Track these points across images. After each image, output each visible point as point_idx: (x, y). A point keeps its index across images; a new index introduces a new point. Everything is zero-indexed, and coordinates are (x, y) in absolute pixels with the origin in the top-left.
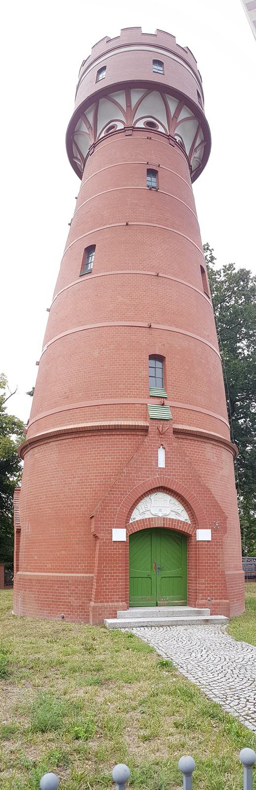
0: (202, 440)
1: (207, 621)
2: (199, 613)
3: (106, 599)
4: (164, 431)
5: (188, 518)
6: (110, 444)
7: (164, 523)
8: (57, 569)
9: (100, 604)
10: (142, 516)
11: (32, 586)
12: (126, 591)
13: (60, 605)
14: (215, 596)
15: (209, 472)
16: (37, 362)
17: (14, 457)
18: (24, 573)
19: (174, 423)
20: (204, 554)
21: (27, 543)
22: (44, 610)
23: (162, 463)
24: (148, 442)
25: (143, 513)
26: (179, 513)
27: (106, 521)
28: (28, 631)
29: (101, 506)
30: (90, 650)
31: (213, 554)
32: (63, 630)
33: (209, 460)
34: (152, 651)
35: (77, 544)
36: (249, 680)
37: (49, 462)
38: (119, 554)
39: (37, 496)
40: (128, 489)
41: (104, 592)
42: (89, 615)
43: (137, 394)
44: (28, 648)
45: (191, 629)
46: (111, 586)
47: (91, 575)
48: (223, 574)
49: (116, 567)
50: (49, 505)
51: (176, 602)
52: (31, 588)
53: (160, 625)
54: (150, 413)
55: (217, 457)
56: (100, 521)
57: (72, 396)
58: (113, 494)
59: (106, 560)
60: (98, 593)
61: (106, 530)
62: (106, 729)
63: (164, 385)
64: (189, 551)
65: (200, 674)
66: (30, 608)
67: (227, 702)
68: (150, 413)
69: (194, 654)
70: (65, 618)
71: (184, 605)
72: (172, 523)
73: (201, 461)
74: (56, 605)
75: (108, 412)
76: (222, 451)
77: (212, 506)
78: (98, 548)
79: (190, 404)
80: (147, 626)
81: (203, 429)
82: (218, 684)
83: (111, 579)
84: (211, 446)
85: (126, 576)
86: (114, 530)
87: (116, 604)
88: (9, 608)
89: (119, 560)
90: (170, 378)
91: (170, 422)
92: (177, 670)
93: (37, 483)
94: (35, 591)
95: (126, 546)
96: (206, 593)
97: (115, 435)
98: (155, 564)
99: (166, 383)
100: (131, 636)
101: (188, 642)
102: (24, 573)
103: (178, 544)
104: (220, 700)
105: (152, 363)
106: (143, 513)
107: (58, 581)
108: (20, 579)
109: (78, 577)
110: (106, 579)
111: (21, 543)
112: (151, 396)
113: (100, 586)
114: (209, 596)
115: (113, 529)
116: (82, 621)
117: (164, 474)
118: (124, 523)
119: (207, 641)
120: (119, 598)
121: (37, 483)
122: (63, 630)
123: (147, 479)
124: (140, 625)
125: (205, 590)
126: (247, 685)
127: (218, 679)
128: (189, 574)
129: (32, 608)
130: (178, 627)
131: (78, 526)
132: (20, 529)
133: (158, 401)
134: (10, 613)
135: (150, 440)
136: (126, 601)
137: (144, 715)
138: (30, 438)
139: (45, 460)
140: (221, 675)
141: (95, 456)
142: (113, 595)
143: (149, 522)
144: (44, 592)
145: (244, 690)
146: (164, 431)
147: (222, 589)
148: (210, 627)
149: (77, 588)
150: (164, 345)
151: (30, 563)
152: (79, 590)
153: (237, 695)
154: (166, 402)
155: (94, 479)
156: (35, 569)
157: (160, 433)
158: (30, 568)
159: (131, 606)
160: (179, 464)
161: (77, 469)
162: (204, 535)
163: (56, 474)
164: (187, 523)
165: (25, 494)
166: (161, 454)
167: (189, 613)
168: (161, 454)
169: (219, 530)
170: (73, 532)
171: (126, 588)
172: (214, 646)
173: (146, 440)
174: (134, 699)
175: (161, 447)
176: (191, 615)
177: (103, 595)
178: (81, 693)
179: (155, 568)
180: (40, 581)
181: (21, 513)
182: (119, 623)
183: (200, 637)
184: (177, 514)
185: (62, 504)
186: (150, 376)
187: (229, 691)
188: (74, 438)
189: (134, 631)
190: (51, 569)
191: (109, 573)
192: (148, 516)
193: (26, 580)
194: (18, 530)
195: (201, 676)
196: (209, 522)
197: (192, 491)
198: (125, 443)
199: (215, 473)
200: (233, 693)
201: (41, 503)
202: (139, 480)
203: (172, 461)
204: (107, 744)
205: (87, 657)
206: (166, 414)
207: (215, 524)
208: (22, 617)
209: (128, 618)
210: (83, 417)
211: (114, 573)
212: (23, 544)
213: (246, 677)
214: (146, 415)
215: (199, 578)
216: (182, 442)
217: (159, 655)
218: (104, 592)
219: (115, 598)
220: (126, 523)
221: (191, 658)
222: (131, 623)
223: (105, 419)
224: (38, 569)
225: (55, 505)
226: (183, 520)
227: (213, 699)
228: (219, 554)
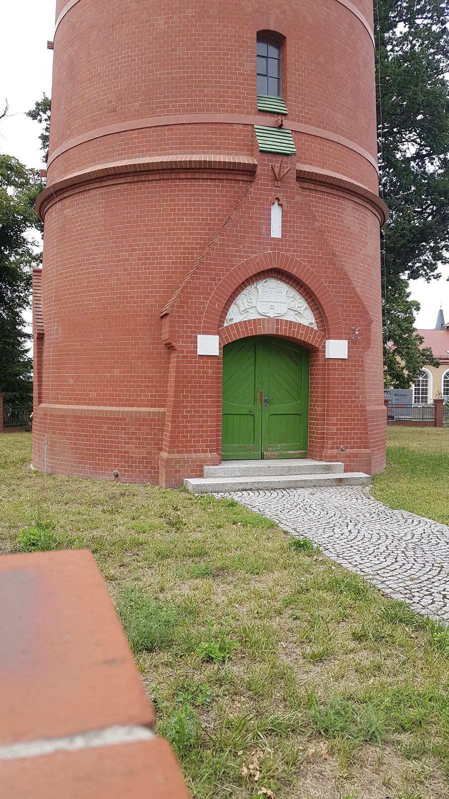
0: (340, 193)
1: (340, 481)
2: (328, 469)
4: (282, 174)
5: (313, 321)
6: (191, 195)
7: (277, 329)
8: (107, 400)
9: (177, 456)
10: (244, 316)
11: (66, 425)
12: (218, 436)
13: (111, 456)
14: (350, 443)
15: (346, 249)
16: (49, 43)
17: (15, 220)
18: (52, 406)
19: (298, 161)
20: (337, 379)
21: (56, 355)
22: (86, 463)
23: (276, 231)
24: (255, 194)
25: (246, 311)
26: (301, 312)
27: (187, 322)
28: (68, 495)
29: (179, 297)
30: (176, 525)
31: (349, 379)
32: (123, 495)
33: (348, 228)
34: (273, 526)
35: (139, 358)
36: (433, 565)
37: (89, 223)
38: (208, 377)
39: (73, 280)
40: (222, 270)
41: (183, 437)
42: (157, 473)
43: (236, 107)
44: (78, 522)
45: (320, 494)
47: (162, 410)
48: (363, 410)
49: (202, 397)
50: (92, 296)
51: (292, 452)
52: (64, 430)
53: (271, 488)
54: (259, 141)
55: (359, 224)
56: (178, 322)
57: (122, 108)
58: (198, 279)
59: (187, 387)
60: (173, 439)
62: (249, 646)
63: (282, 91)
64: (312, 374)
65: (357, 558)
66: (62, 460)
67: (416, 599)
68: (259, 141)
69: (337, 530)
71: (304, 457)
72: (290, 329)
73: (337, 229)
74: (105, 456)
75: (188, 138)
76: (367, 215)
77: (350, 302)
78: (173, 364)
79: (325, 128)
80: (251, 490)
81: (342, 174)
82: (391, 573)
83: (194, 416)
84: (352, 205)
85: (218, 411)
86: (200, 337)
87: (202, 455)
88: (23, 461)
89: (208, 387)
90: (293, 78)
91: (292, 158)
92: (319, 552)
93: (71, 258)
94: (70, 435)
95: (218, 363)
96: (338, 439)
97: (199, 179)
98: (261, 393)
99: (286, 87)
100: (233, 504)
101: (322, 512)
102: (52, 406)
103: (295, 362)
104: (403, 596)
105: (262, 48)
106: (246, 311)
107: (108, 419)
108: (45, 415)
109: (140, 412)
110: (186, 417)
111: (45, 354)
112: (260, 110)
113: (178, 427)
114: (342, 443)
116: (148, 481)
117: (279, 249)
118: (216, 326)
119: (349, 510)
121: (71, 258)
122: (123, 495)
123: (253, 256)
124: (241, 487)
125: (336, 434)
126: (434, 573)
127: (388, 566)
128: (311, 410)
129: (66, 461)
130: (299, 490)
131: (140, 330)
132: (43, 334)
133: (272, 120)
134: (28, 468)
135: (258, 189)
136: (217, 450)
137: (298, 622)
138: (53, 183)
139: (82, 221)
140: (390, 560)
141: (167, 215)
143: (255, 327)
144: (85, 436)
145: (432, 580)
146: (282, 174)
147: (361, 434)
148: (347, 490)
149: (139, 429)
150: (284, 13)
151: (61, 390)
152: (143, 434)
153: (426, 588)
154: (287, 123)
155: (166, 253)
156: (70, 399)
157: (276, 178)
158: (62, 399)
159: (224, 459)
160: (304, 233)
161: (137, 236)
162: (336, 349)
163: (102, 244)
164: (312, 329)
165: (51, 277)
166: (276, 214)
167: (312, 470)
168: (276, 214)
169: (357, 344)
170: (132, 339)
171: (218, 431)
172: (362, 517)
173: (251, 190)
174: (274, 598)
175: (276, 204)
176: (316, 472)
177: (182, 442)
178: (186, 591)
179: (261, 401)
180: (78, 418)
181: (46, 308)
182: (209, 485)
183: (337, 504)
184: (298, 313)
185: (114, 294)
186: (258, 74)
187: (411, 583)
189: (236, 497)
190: (96, 399)
191: (192, 407)
192: (252, 316)
193: (57, 416)
194: (40, 336)
195: (361, 562)
196: (345, 329)
197: (322, 277)
198: (215, 193)
199: (355, 251)
200: (418, 585)
201: (79, 293)
202: (240, 256)
203: (293, 227)
204: (260, 670)
205: (174, 535)
206: (283, 143)
207: (354, 330)
208: (50, 475)
209: (222, 476)
210: (143, 146)
212: (48, 356)
213: (428, 562)
214: (252, 146)
215: (328, 415)
216: (309, 196)
217: (286, 533)
218: (183, 437)
219: (201, 445)
220: (219, 326)
221: (336, 536)
222: (227, 484)
223: (182, 150)
224: (75, 399)
225: (102, 295)
226: (305, 323)
227: (392, 596)
228: (357, 379)
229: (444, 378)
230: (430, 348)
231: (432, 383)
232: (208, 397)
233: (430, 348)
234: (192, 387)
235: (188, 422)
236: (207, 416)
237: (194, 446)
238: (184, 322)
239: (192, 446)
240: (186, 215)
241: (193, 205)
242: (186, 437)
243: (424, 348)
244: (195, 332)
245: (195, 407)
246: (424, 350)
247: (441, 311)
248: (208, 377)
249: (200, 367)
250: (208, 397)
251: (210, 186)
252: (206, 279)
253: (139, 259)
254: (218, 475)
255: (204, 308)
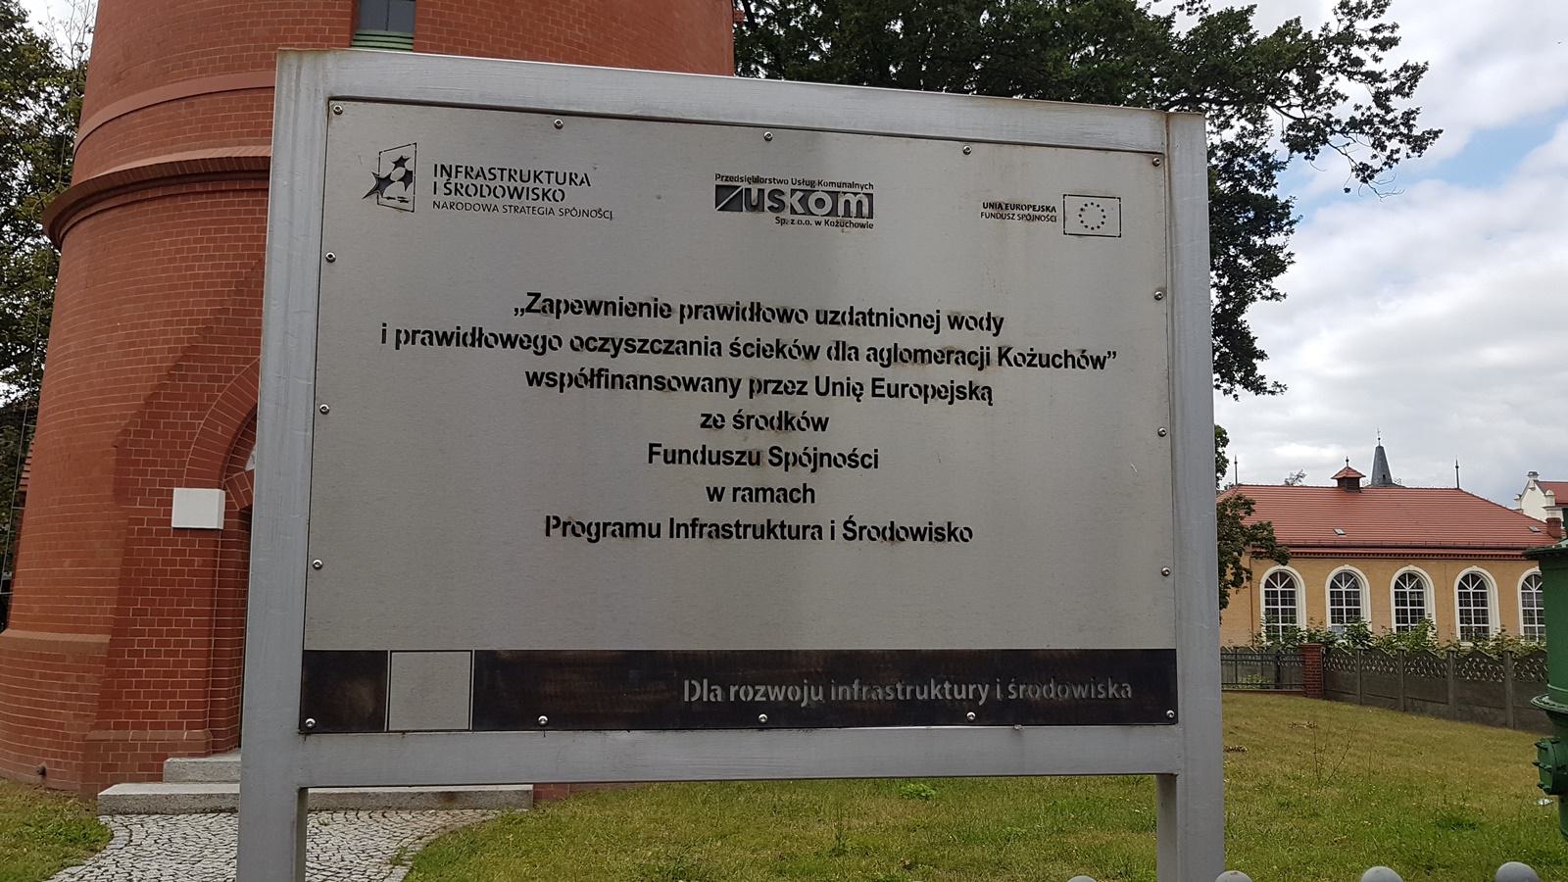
3: (135, 715)
38: (191, 573)
40: (236, 360)
46: (156, 674)
49: (178, 613)
58: (183, 378)
61: (153, 493)
70: (48, 777)
115: (176, 490)
120: (182, 715)
124: (209, 804)
142: (163, 706)
188: (214, 192)
211: (170, 633)
218: (130, 695)
222: (176, 796)
229: (1523, 589)
230: (1269, 524)
231: (1304, 598)
232: (189, 613)
233: (1269, 524)
234: (155, 592)
235: (143, 664)
236: (186, 654)
237: (154, 715)
238: (147, 463)
239: (147, 715)
240: (198, 259)
241: (213, 240)
242: (136, 695)
243: (1256, 522)
244: (172, 484)
245: (159, 633)
246: (1254, 527)
247: (1380, 450)
248: (191, 573)
249: (176, 553)
250: (189, 613)
251: (246, 203)
252: (199, 378)
253: (121, 346)
254: (189, 777)
255: (192, 435)
